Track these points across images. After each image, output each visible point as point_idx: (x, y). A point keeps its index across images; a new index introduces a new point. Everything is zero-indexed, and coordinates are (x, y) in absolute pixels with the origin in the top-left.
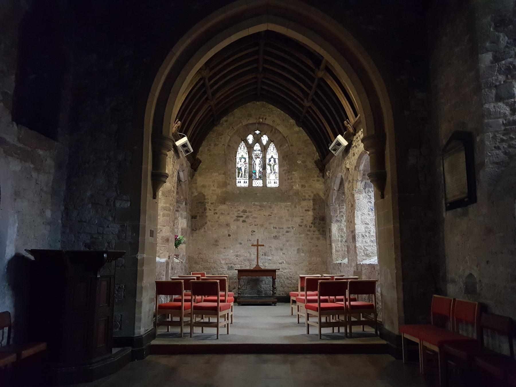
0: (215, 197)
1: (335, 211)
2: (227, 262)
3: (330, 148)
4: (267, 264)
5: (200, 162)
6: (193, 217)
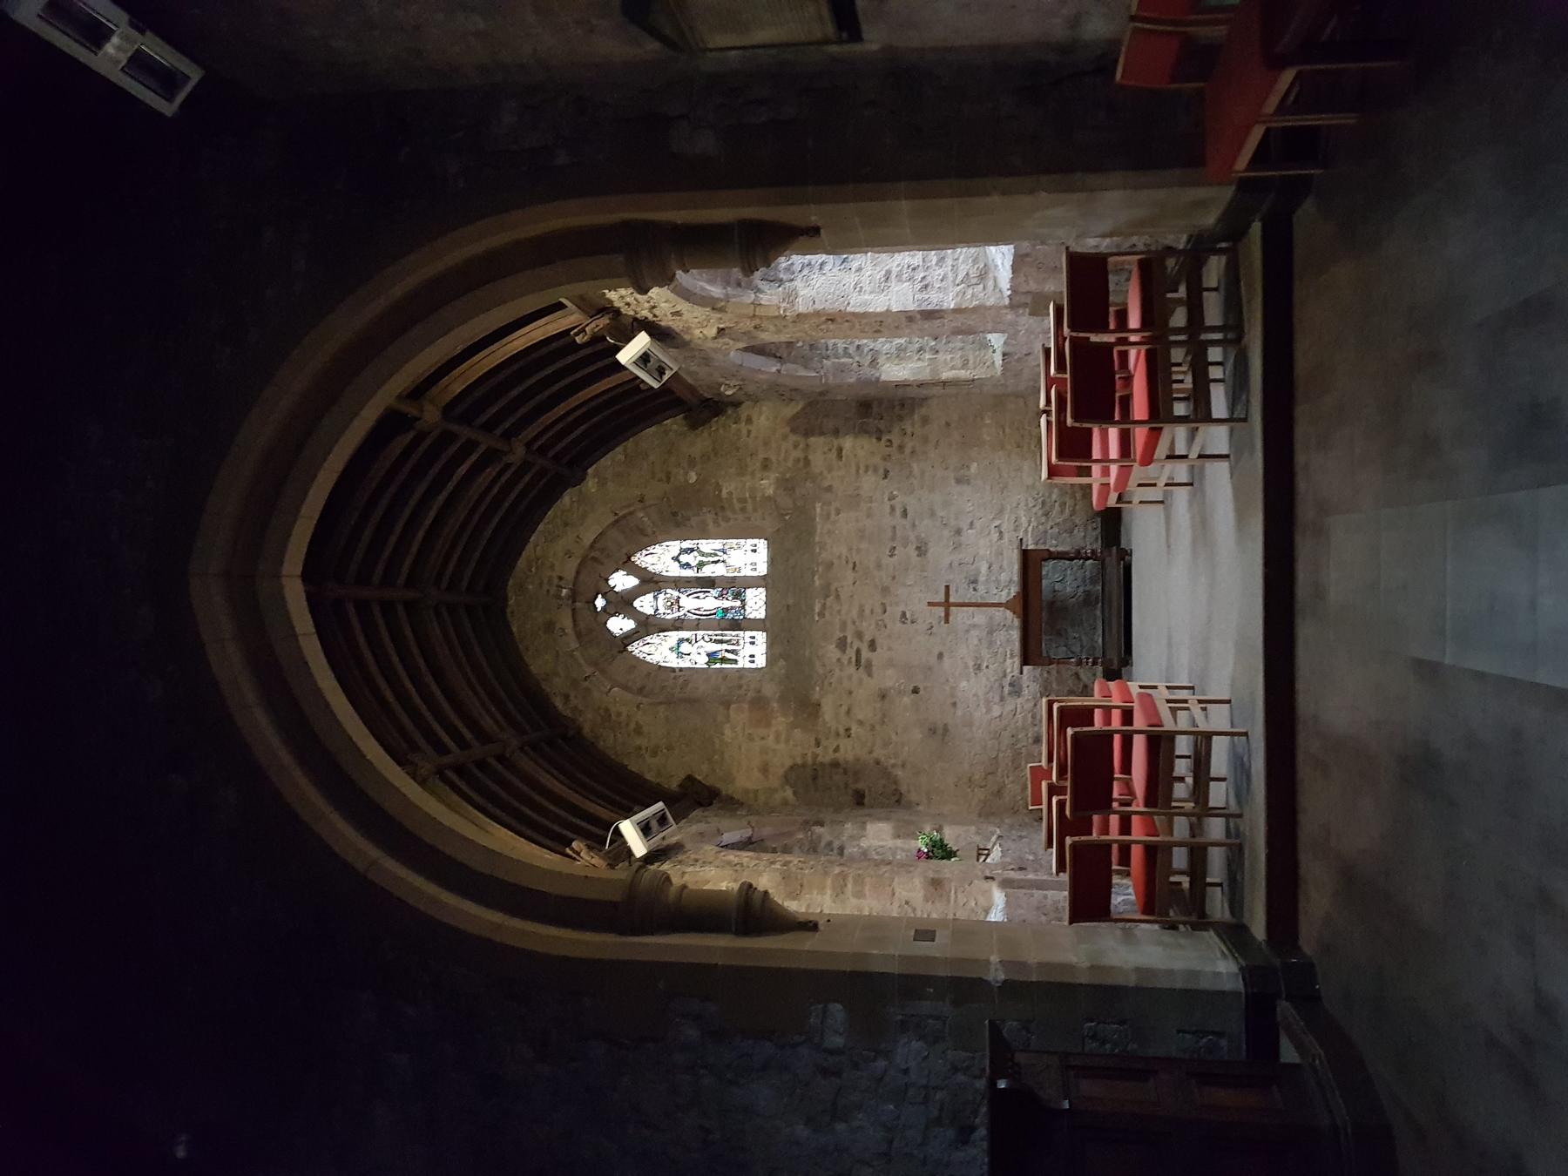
1: (842, 369)
2: (997, 699)
3: (656, 385)
4: (1004, 577)
5: (690, 778)
6: (859, 800)
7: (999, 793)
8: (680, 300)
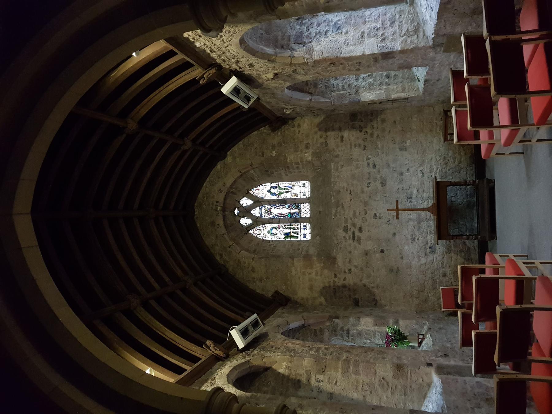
0: (326, 271)
1: (341, 97)
2: (423, 255)
3: (246, 107)
4: (425, 195)
5: (277, 292)
6: (356, 303)
7: (426, 301)
8: (250, 56)
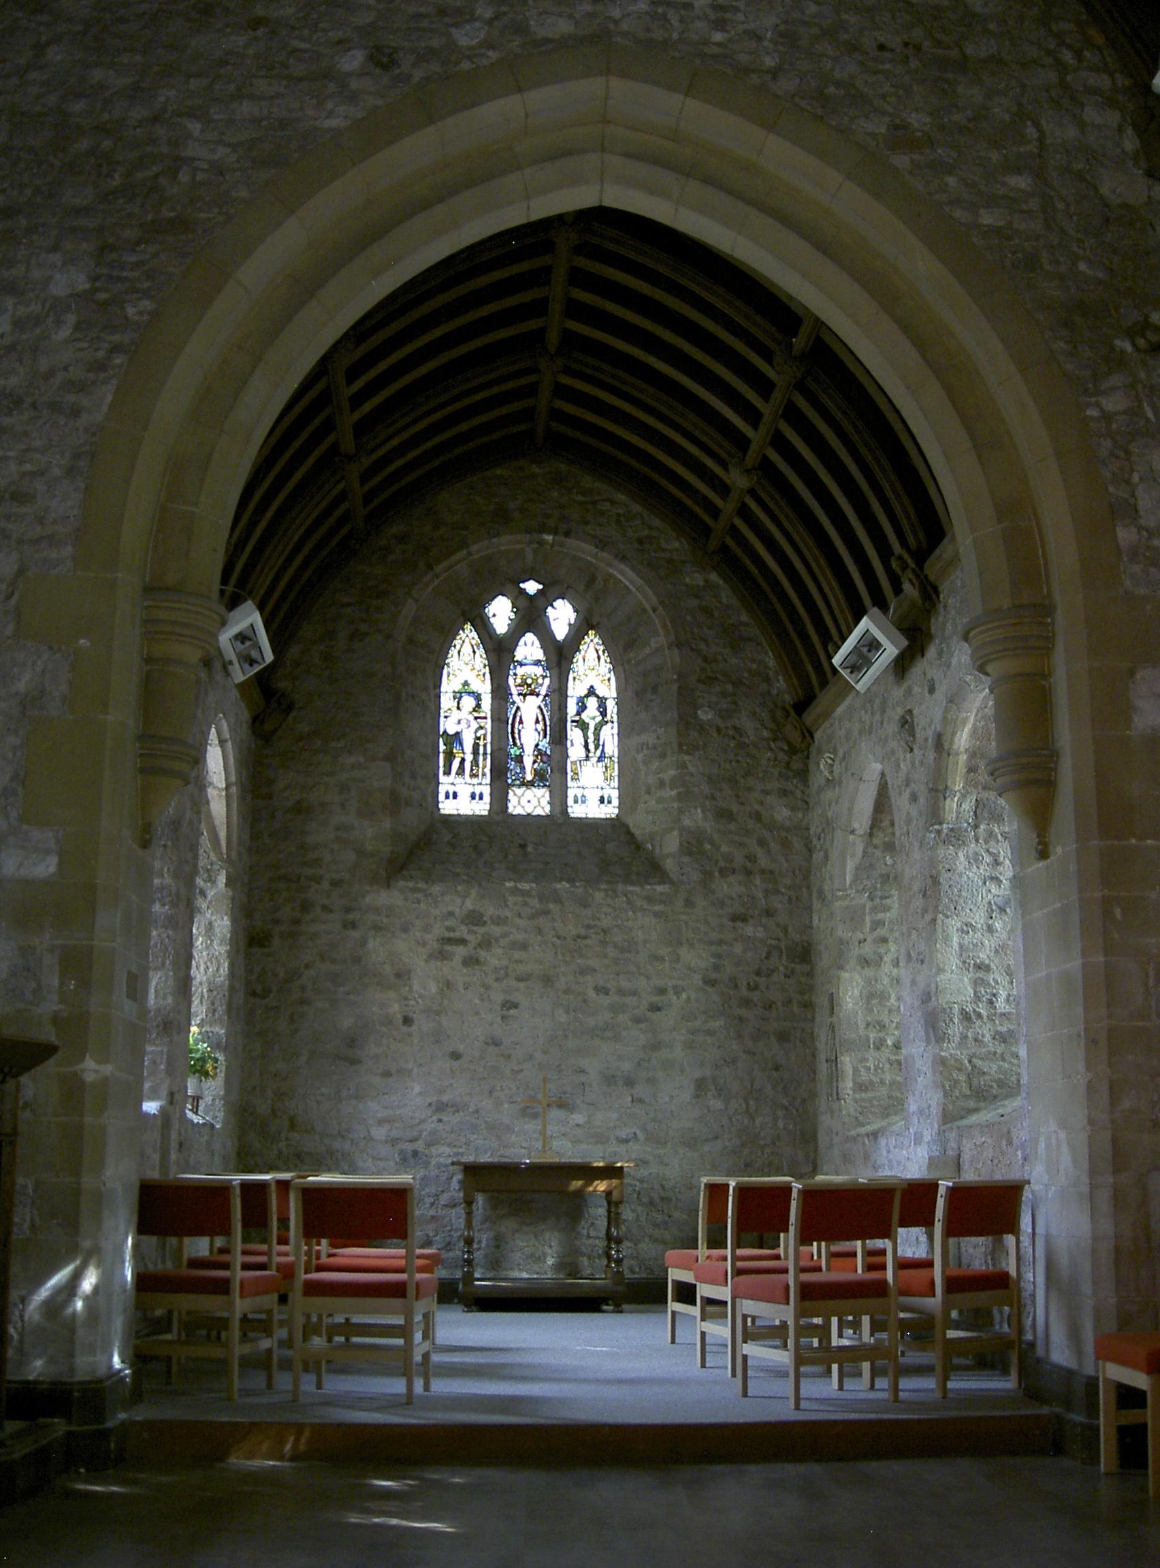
2: (394, 1134)
3: (837, 660)
